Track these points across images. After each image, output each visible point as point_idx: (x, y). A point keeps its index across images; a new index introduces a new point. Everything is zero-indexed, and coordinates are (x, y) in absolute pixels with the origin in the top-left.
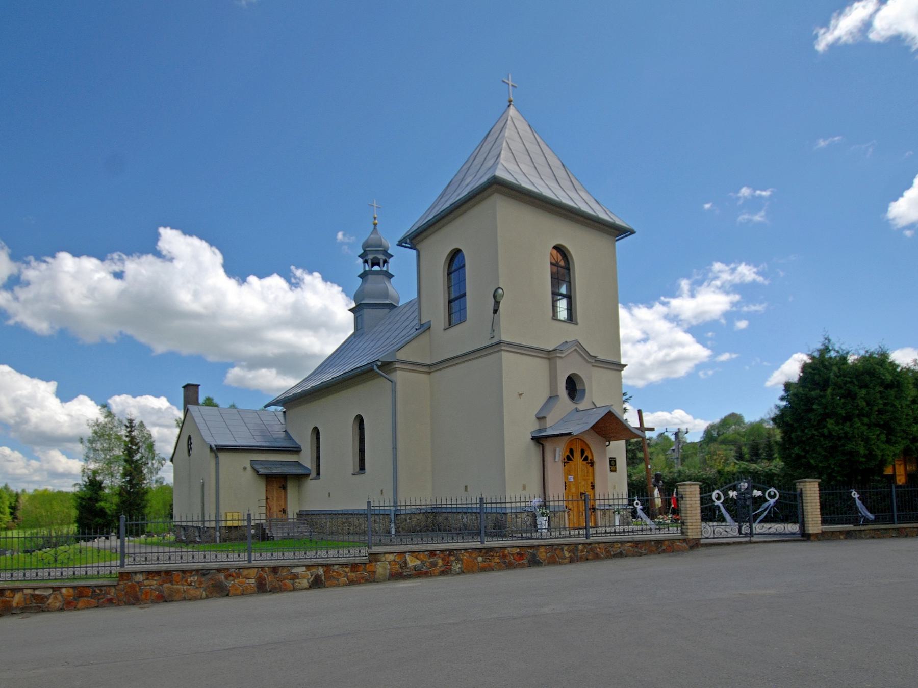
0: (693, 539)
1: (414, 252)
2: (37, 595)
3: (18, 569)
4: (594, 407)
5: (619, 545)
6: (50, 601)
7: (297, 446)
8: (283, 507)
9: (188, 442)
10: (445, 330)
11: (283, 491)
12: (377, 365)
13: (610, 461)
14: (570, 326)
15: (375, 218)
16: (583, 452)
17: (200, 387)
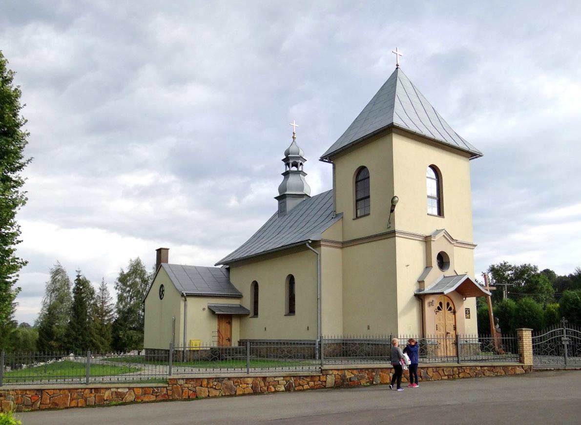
0: (527, 366)
1: (331, 165)
2: (119, 392)
3: (107, 375)
4: (456, 275)
5: (480, 368)
6: (127, 396)
7: (240, 294)
8: (229, 337)
9: (160, 289)
10: (354, 219)
11: (229, 325)
12: (309, 243)
13: (466, 311)
14: (440, 219)
15: (294, 133)
16: (448, 304)
17: (169, 250)
